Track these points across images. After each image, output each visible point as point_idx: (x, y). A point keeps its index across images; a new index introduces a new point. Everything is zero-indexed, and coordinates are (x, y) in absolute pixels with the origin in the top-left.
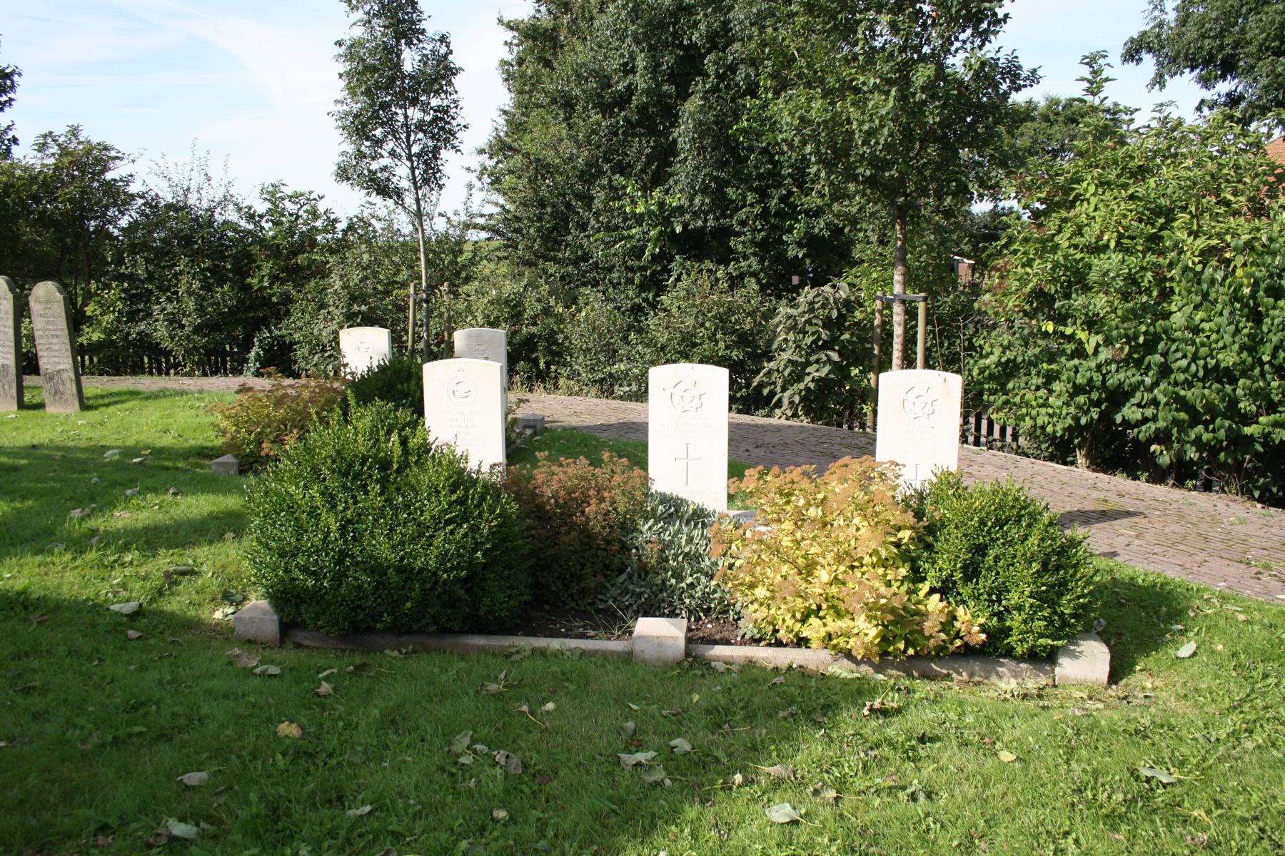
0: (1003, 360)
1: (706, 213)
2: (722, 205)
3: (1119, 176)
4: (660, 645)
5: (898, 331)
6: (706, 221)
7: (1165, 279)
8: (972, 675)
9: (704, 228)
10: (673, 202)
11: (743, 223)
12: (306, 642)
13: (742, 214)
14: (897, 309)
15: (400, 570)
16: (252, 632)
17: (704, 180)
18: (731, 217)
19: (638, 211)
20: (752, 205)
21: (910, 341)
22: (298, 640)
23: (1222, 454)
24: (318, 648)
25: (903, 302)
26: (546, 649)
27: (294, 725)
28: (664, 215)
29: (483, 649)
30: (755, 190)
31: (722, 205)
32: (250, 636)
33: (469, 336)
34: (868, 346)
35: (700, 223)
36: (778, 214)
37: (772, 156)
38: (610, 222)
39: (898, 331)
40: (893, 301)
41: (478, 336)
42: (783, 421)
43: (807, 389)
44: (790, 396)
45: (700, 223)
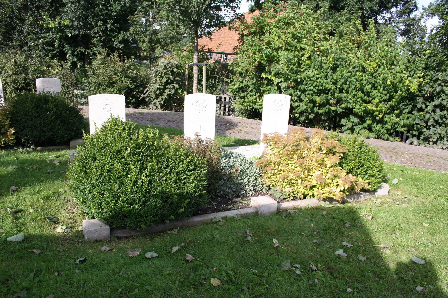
0: (240, 86)
1: (79, 29)
2: (88, 26)
3: (283, 25)
4: (269, 207)
5: (195, 77)
6: (79, 32)
7: (301, 60)
8: (354, 199)
9: (78, 35)
10: (67, 22)
11: (95, 33)
12: (120, 235)
13: (96, 29)
14: (195, 69)
15: (178, 195)
16: (96, 236)
17: (79, 15)
18: (90, 31)
19: (50, 26)
20: (100, 26)
21: (200, 82)
22: (116, 235)
23: (323, 116)
24: (127, 237)
25: (197, 65)
26: (226, 217)
27: (216, 279)
28: (61, 29)
29: (204, 223)
30: (102, 20)
31: (88, 26)
32: (95, 239)
33: (43, 82)
34: (184, 82)
35: (77, 32)
36: (111, 30)
37: (107, 7)
38: (34, 30)
39: (195, 77)
40: (194, 65)
41: (47, 81)
42: (154, 111)
43: (166, 99)
44: (159, 102)
45: (77, 32)
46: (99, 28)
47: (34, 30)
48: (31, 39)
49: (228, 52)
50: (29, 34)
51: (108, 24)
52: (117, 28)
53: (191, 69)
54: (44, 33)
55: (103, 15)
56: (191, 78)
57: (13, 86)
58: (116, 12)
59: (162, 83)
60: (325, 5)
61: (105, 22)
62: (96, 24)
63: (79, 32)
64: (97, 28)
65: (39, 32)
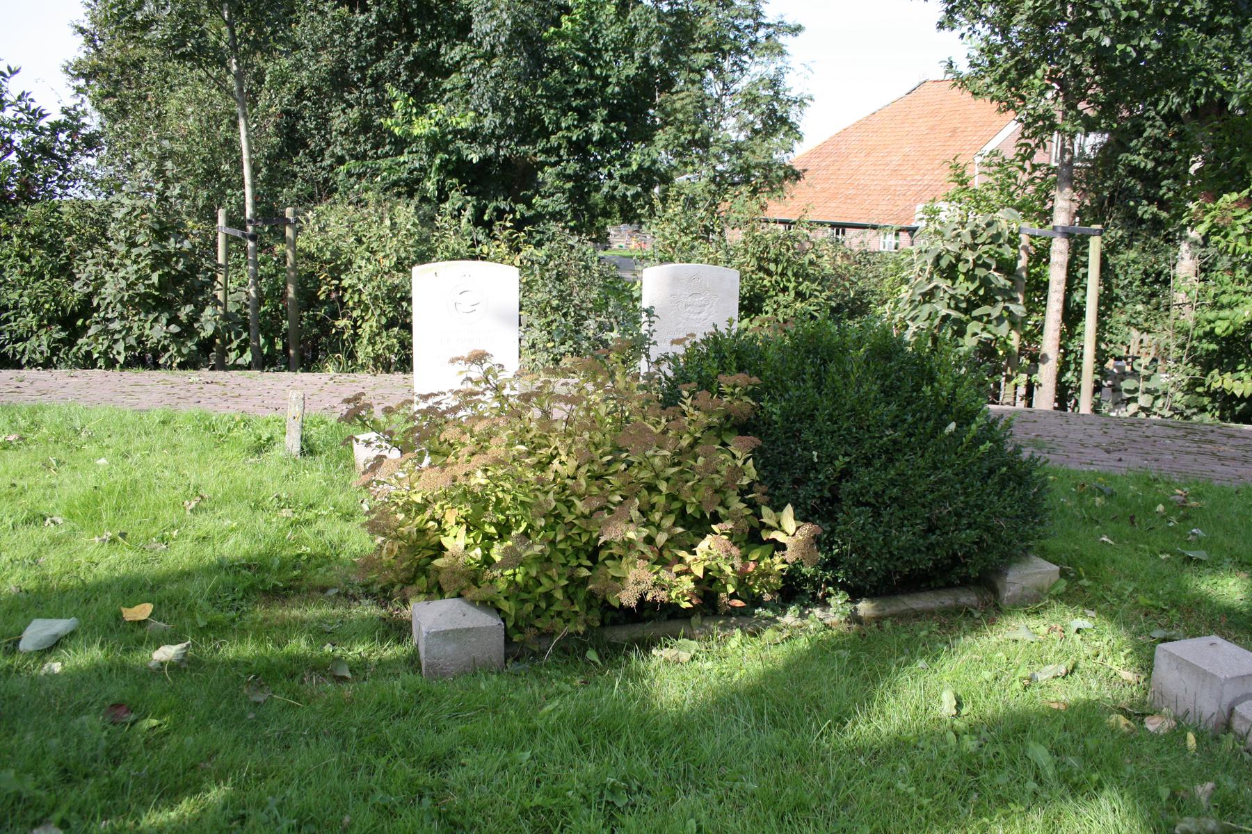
1: (499, 138)
14: (1059, 251)
20: (568, 128)
33: (675, 279)
36: (604, 143)
37: (592, 69)
41: (692, 279)
46: (565, 133)
47: (354, 149)
48: (349, 174)
49: (848, 221)
50: (341, 160)
51: (594, 120)
52: (620, 133)
53: (1041, 256)
54: (386, 155)
55: (578, 93)
56: (1039, 286)
57: (383, 313)
58: (618, 84)
59: (958, 301)
60: (319, 32)
61: (584, 116)
62: (558, 123)
63: (498, 149)
64: (560, 134)
65: (370, 154)
